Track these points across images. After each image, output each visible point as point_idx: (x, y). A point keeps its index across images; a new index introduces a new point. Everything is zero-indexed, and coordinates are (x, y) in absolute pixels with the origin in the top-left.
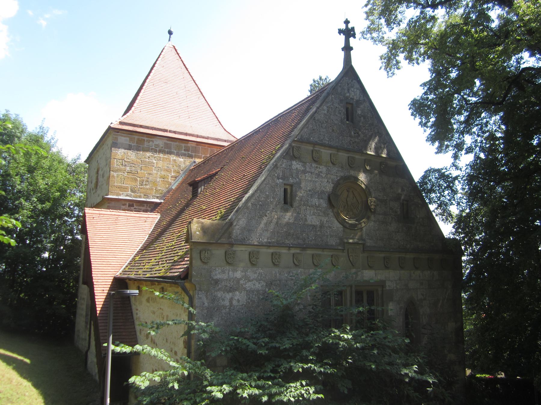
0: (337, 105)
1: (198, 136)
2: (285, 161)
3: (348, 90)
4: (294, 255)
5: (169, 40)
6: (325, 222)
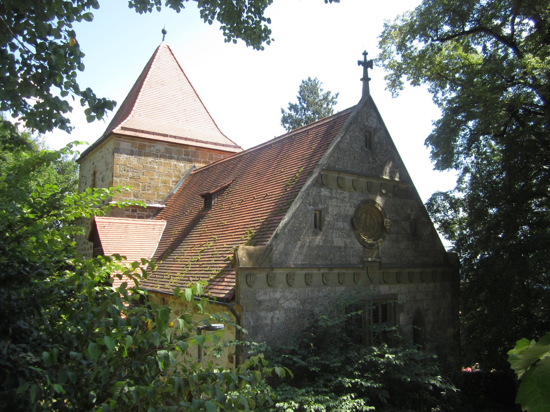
0: (357, 134)
1: (197, 141)
2: (315, 188)
3: (367, 119)
4: (323, 274)
5: (163, 40)
6: (348, 243)
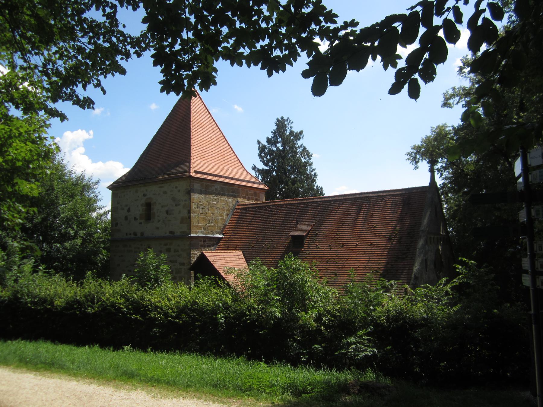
1: (232, 179)
